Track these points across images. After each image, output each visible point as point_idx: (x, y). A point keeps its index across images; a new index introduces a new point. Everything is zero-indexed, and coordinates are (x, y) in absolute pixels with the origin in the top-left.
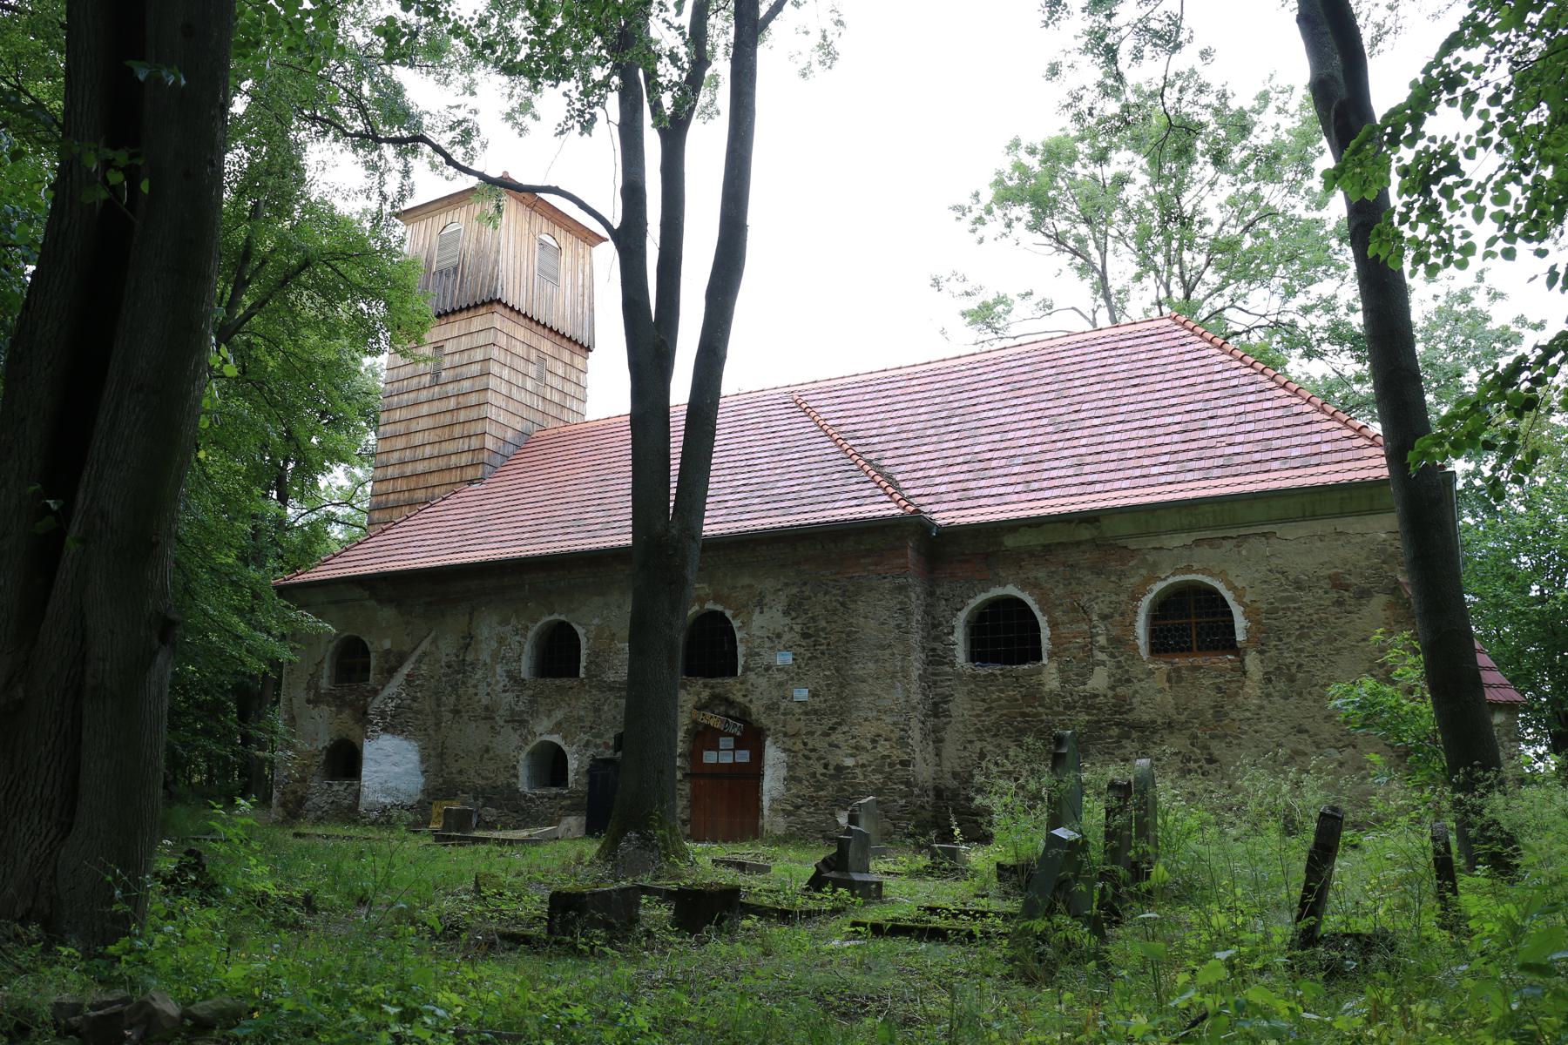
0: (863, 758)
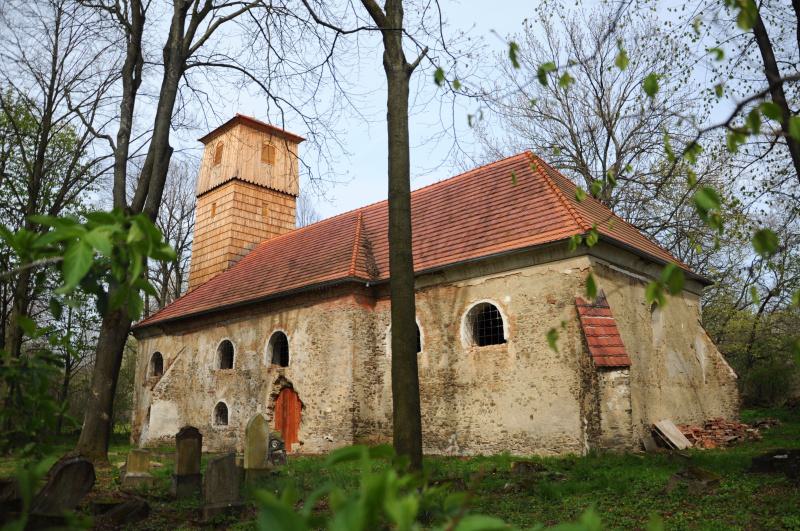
0: (335, 407)
